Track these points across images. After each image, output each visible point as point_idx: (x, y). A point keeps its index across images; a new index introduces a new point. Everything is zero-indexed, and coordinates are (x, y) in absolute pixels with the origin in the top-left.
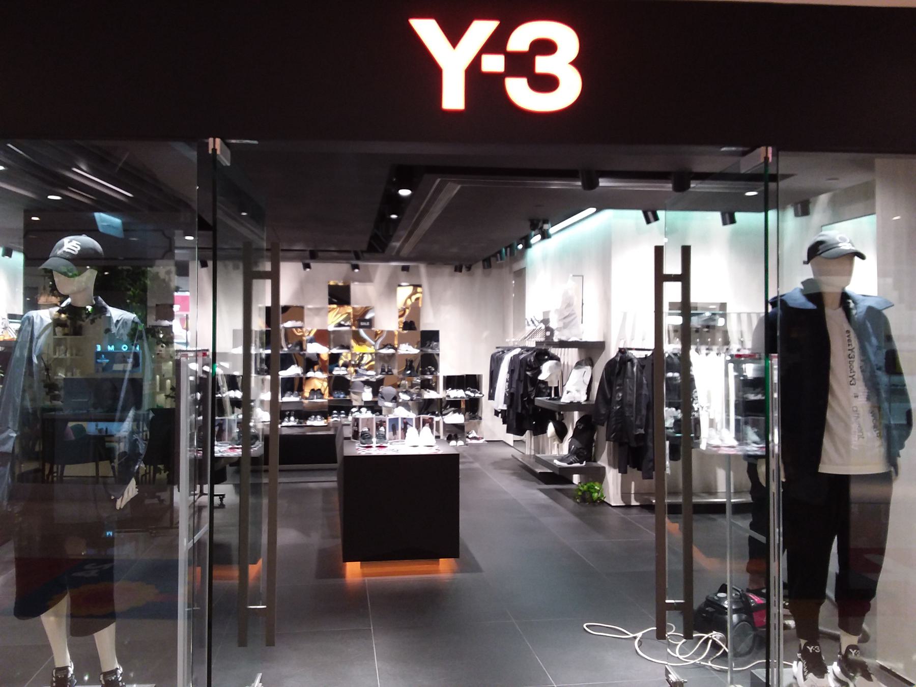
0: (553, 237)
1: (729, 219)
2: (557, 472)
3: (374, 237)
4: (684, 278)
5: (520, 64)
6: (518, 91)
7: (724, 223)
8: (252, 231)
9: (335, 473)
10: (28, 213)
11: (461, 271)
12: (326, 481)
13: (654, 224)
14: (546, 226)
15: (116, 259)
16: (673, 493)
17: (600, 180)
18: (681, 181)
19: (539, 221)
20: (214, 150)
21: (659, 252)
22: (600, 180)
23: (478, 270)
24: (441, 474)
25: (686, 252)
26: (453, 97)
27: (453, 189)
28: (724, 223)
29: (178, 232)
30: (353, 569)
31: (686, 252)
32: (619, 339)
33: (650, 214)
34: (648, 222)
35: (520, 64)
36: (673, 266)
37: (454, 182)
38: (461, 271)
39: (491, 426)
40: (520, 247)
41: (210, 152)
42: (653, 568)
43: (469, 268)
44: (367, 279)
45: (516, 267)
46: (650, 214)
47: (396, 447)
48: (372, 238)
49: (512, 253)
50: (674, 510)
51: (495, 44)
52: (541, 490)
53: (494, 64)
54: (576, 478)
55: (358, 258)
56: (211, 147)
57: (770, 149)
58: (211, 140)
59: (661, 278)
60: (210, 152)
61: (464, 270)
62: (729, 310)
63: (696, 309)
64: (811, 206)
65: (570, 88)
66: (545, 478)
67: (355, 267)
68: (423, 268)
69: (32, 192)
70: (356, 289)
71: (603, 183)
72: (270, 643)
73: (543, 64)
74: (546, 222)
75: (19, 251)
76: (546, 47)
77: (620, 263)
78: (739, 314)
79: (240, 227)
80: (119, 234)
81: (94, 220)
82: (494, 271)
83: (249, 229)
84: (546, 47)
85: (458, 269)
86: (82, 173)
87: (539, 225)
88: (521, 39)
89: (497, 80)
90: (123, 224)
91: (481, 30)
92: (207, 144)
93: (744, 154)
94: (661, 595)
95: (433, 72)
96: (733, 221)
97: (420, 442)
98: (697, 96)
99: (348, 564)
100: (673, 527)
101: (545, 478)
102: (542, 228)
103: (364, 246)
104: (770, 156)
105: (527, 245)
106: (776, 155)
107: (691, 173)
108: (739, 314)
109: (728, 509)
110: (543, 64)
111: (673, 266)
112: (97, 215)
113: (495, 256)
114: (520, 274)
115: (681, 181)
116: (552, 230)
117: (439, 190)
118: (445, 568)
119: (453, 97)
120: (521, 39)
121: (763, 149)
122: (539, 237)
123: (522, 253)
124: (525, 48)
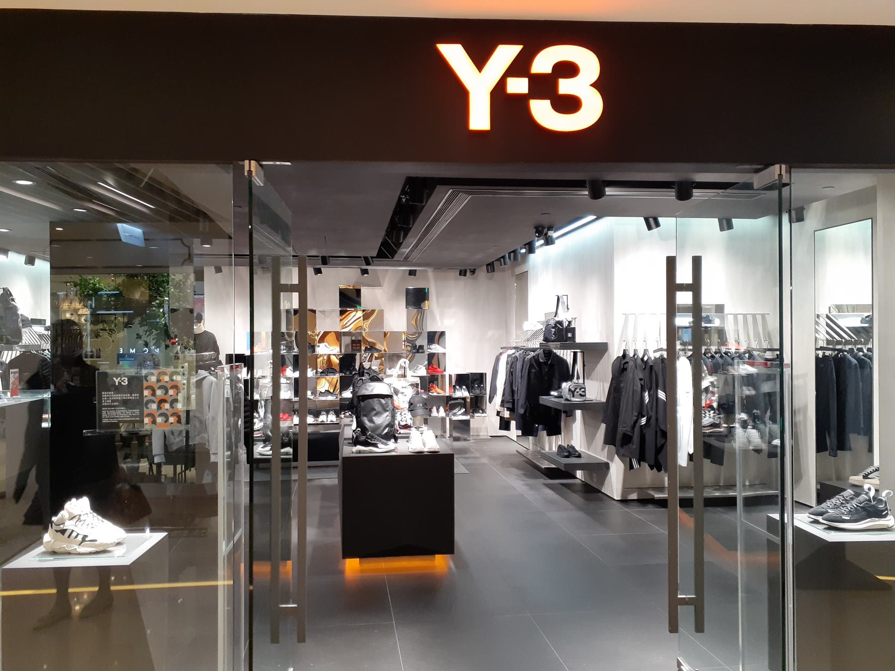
0: (557, 241)
1: (726, 224)
2: (563, 469)
3: (384, 244)
4: (695, 287)
5: (543, 86)
6: (542, 112)
7: (722, 229)
8: (270, 239)
9: (337, 469)
10: (53, 225)
11: (465, 275)
12: (330, 479)
13: (655, 231)
14: (550, 233)
15: (134, 267)
16: (684, 487)
17: (607, 189)
18: (684, 191)
19: (543, 228)
20: (250, 172)
21: (671, 263)
22: (607, 189)
23: (482, 273)
24: (436, 470)
25: (697, 262)
26: (480, 118)
27: (464, 200)
28: (722, 229)
29: (197, 241)
30: (352, 565)
31: (697, 262)
32: (623, 339)
33: (651, 220)
34: (650, 228)
35: (543, 86)
36: (684, 276)
37: (465, 192)
38: (465, 275)
39: (487, 421)
40: (523, 251)
42: (665, 561)
43: (473, 272)
44: (376, 284)
45: (519, 270)
46: (651, 220)
47: (401, 448)
48: (382, 244)
49: (515, 258)
50: (686, 504)
51: (519, 67)
52: (548, 486)
53: (518, 86)
54: (579, 474)
55: (368, 264)
56: (247, 168)
57: (783, 166)
58: (247, 162)
59: (673, 287)
61: (468, 273)
62: (726, 311)
63: (769, 336)
64: (805, 212)
65: (592, 110)
66: (551, 473)
67: (364, 272)
68: (430, 272)
69: (59, 205)
70: (366, 293)
71: (609, 191)
72: (302, 639)
73: (565, 86)
74: (550, 228)
75: (44, 259)
76: (568, 69)
77: (622, 267)
78: (735, 316)
79: (267, 242)
80: (140, 243)
81: (117, 231)
82: (496, 274)
83: (265, 236)
84: (568, 69)
85: (463, 273)
86: (108, 187)
87: (543, 232)
88: (544, 62)
89: (522, 101)
90: (144, 233)
91: (505, 54)
93: (757, 171)
94: (673, 588)
95: (461, 94)
96: (730, 226)
97: (422, 440)
98: (714, 116)
99: (348, 560)
100: (685, 519)
101: (551, 473)
102: (546, 234)
103: (375, 254)
104: (783, 172)
105: (531, 249)
106: (789, 172)
107: (694, 182)
108: (735, 316)
109: (740, 503)
110: (565, 86)
111: (684, 276)
112: (119, 225)
113: (499, 260)
114: (523, 278)
115: (684, 191)
116: (555, 235)
117: (449, 201)
118: (440, 562)
119: (480, 118)
120: (544, 62)
121: (777, 166)
122: (542, 242)
123: (524, 256)
124: (548, 70)
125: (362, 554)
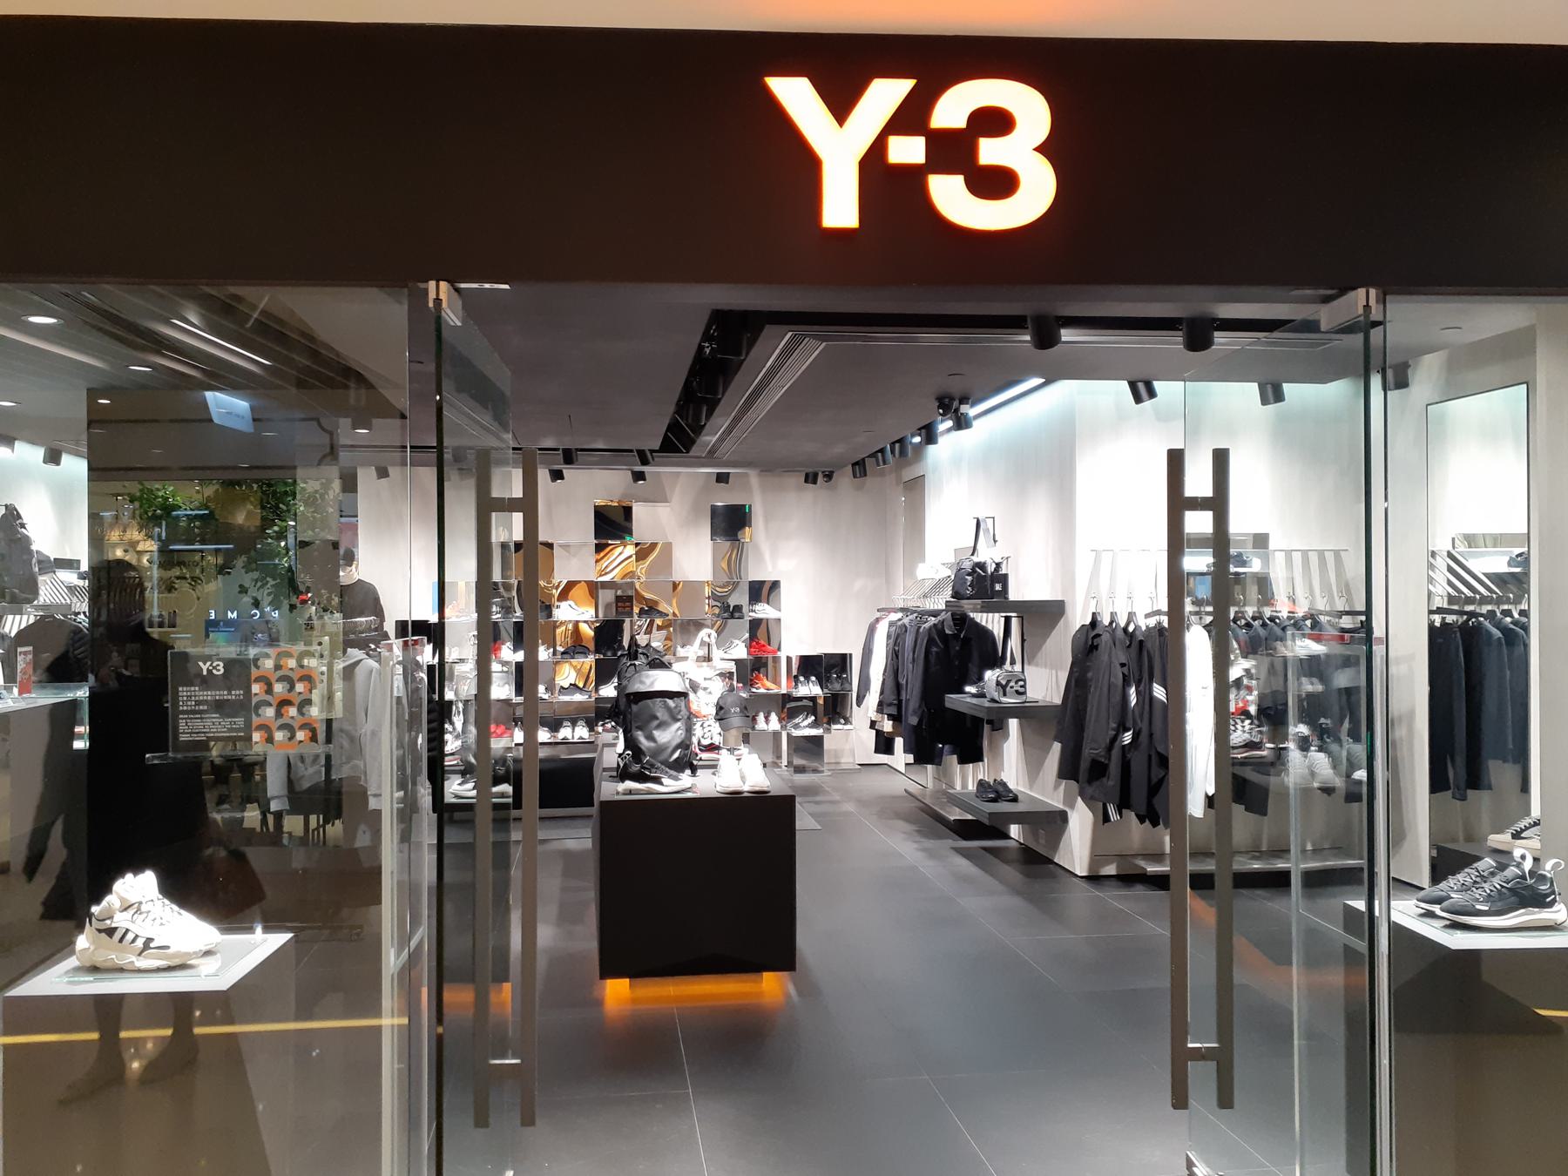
0: (975, 423)
1: (1272, 393)
2: (986, 821)
3: (673, 427)
4: (1218, 503)
5: (952, 151)
6: (950, 196)
7: (1265, 401)
8: (474, 420)
9: (591, 823)
10: (93, 394)
11: (815, 482)
12: (579, 839)
13: (1148, 404)
14: (964, 409)
15: (235, 468)
16: (1198, 854)
17: (1063, 331)
18: (1198, 335)
19: (952, 399)
20: (438, 301)
21: (1176, 461)
22: (1063, 331)
23: (845, 479)
24: (763, 824)
25: (1221, 459)
26: (840, 207)
27: (812, 351)
28: (1265, 401)
29: (345, 423)
30: (617, 991)
31: (1221, 459)
32: (1092, 595)
33: (1141, 386)
34: (1138, 399)
35: (952, 151)
36: (1198, 483)
37: (815, 337)
38: (815, 482)
39: (853, 739)
40: (917, 439)
41: (431, 304)
42: (1166, 983)
43: (829, 476)
44: (659, 497)
45: (908, 474)
46: (1141, 386)
47: (703, 784)
48: (669, 428)
49: (903, 453)
50: (1202, 882)
51: (909, 118)
52: (959, 851)
53: (907, 150)
54: (1015, 830)
55: (645, 462)
56: (432, 295)
57: (1373, 292)
58: (432, 284)
59: (1178, 503)
60: (431, 304)
61: (820, 479)
62: (1272, 545)
63: (1346, 590)
64: (1410, 372)
65: (1037, 192)
66: (965, 830)
67: (638, 476)
68: (754, 477)
69: (103, 360)
70: (641, 513)
71: (1067, 335)
72: (528, 1120)
73: (991, 152)
74: (964, 400)
75: (78, 454)
76: (995, 121)
77: (1089, 469)
78: (1288, 553)
79: (468, 425)
80: (245, 426)
81: (204, 405)
82: (869, 481)
83: (464, 413)
84: (995, 121)
85: (811, 478)
86: (190, 328)
87: (951, 407)
88: (954, 108)
89: (914, 176)
90: (252, 408)
91: (885, 95)
92: (426, 291)
93: (1326, 300)
94: (1179, 1031)
95: (808, 165)
96: (1279, 397)
97: (740, 772)
98: (1251, 203)
99: (609, 982)
100: (1200, 910)
101: (965, 830)
102: (957, 410)
103: (656, 445)
104: (1372, 302)
105: (930, 436)
106: (1382, 301)
107: (1215, 320)
108: (1288, 553)
109: (1296, 881)
110: (991, 152)
111: (1198, 483)
112: (209, 395)
113: (873, 455)
114: (916, 487)
115: (1198, 335)
116: (972, 411)
117: (788, 352)
118: (771, 986)
119: (840, 207)
120: (954, 108)
121: (1362, 292)
122: (949, 423)
123: (919, 449)
124: (960, 122)
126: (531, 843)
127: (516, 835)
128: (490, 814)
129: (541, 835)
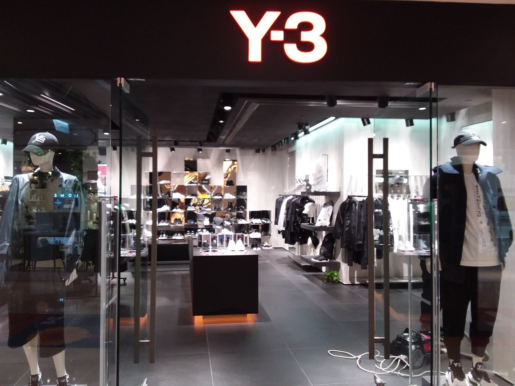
0: (311, 133)
1: (410, 123)
2: (313, 265)
3: (210, 133)
4: (385, 156)
5: (292, 36)
6: (291, 51)
7: (407, 125)
8: (142, 130)
9: (188, 265)
10: (16, 120)
11: (259, 152)
12: (183, 270)
13: (368, 126)
14: (307, 127)
15: (65, 146)
16: (379, 277)
17: (337, 101)
18: (383, 102)
19: (303, 124)
20: (121, 84)
21: (370, 141)
22: (337, 101)
23: (269, 151)
24: (248, 266)
25: (386, 141)
26: (255, 54)
27: (255, 106)
28: (407, 126)
29: (100, 131)
30: (199, 320)
31: (386, 141)
32: (348, 191)
33: (365, 120)
34: (364, 125)
35: (292, 36)
36: (378, 150)
37: (255, 102)
38: (259, 152)
39: (276, 239)
40: (293, 139)
41: (118, 85)
42: (367, 319)
43: (264, 151)
44: (206, 157)
45: (290, 150)
46: (365, 120)
47: (223, 251)
48: (209, 134)
49: (288, 142)
50: (379, 286)
51: (279, 25)
52: (304, 275)
53: (277, 36)
54: (324, 269)
55: (201, 145)
56: (119, 82)
57: (433, 84)
58: (119, 79)
59: (371, 156)
60: (118, 85)
61: (261, 151)
62: (410, 174)
64: (456, 116)
65: (320, 50)
66: (307, 269)
67: (200, 150)
68: (238, 151)
69: (18, 108)
70: (200, 163)
71: (339, 103)
72: (152, 361)
73: (305, 36)
74: (307, 125)
75: (11, 141)
76: (307, 26)
77: (348, 148)
78: (415, 177)
79: (135, 128)
80: (67, 131)
81: (53, 124)
82: (278, 152)
83: (140, 129)
84: (307, 26)
85: (258, 151)
86: (46, 97)
87: (303, 126)
88: (293, 22)
89: (279, 45)
90: (69, 126)
91: (270, 17)
92: (117, 81)
93: (418, 86)
94: (372, 334)
95: (244, 41)
96: (412, 124)
97: (236, 248)
98: (392, 54)
99: (196, 317)
100: (378, 296)
101: (307, 269)
102: (304, 128)
103: (205, 138)
104: (433, 87)
105: (297, 138)
106: (436, 87)
107: (389, 97)
108: (415, 177)
109: (410, 286)
110: (305, 36)
111: (378, 150)
112: (55, 121)
113: (278, 144)
114: (293, 154)
115: (383, 102)
116: (310, 129)
117: (247, 107)
118: (250, 319)
119: (255, 54)
120: (293, 22)
121: (429, 84)
122: (303, 133)
123: (294, 142)
124: (295, 27)
125: (205, 313)
126: (154, 272)
127: (149, 270)
128: (140, 263)
129: (157, 270)
